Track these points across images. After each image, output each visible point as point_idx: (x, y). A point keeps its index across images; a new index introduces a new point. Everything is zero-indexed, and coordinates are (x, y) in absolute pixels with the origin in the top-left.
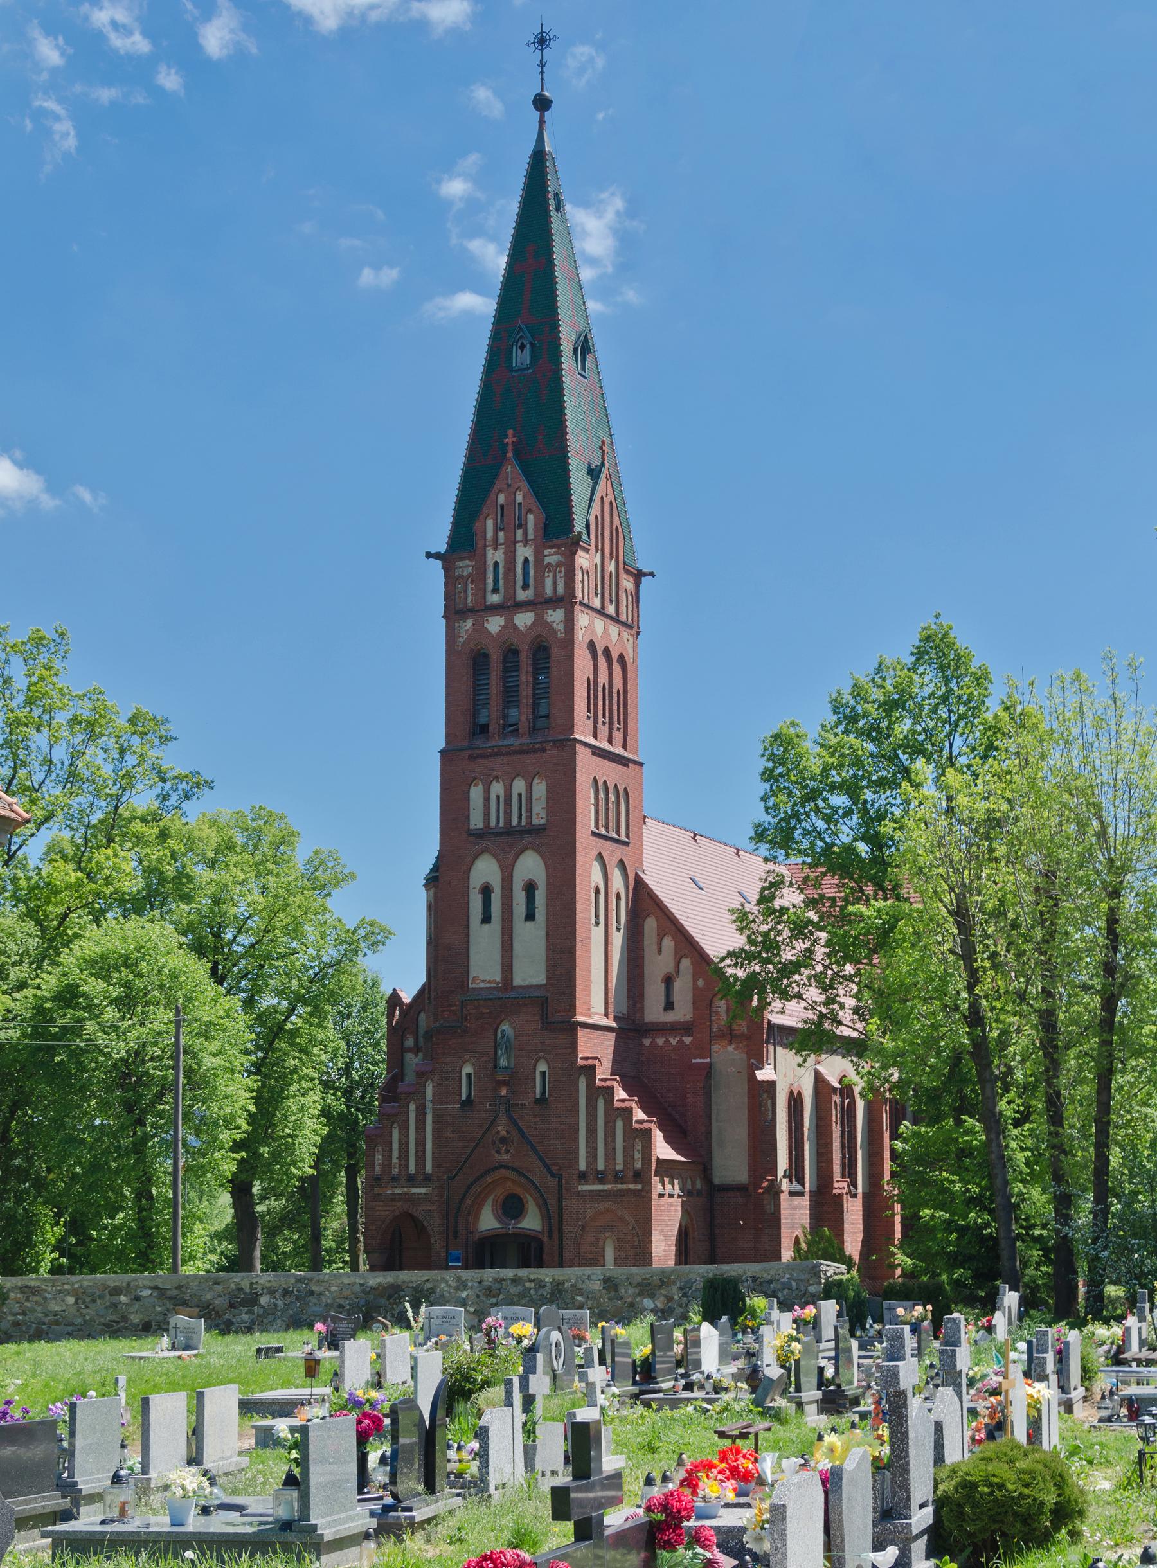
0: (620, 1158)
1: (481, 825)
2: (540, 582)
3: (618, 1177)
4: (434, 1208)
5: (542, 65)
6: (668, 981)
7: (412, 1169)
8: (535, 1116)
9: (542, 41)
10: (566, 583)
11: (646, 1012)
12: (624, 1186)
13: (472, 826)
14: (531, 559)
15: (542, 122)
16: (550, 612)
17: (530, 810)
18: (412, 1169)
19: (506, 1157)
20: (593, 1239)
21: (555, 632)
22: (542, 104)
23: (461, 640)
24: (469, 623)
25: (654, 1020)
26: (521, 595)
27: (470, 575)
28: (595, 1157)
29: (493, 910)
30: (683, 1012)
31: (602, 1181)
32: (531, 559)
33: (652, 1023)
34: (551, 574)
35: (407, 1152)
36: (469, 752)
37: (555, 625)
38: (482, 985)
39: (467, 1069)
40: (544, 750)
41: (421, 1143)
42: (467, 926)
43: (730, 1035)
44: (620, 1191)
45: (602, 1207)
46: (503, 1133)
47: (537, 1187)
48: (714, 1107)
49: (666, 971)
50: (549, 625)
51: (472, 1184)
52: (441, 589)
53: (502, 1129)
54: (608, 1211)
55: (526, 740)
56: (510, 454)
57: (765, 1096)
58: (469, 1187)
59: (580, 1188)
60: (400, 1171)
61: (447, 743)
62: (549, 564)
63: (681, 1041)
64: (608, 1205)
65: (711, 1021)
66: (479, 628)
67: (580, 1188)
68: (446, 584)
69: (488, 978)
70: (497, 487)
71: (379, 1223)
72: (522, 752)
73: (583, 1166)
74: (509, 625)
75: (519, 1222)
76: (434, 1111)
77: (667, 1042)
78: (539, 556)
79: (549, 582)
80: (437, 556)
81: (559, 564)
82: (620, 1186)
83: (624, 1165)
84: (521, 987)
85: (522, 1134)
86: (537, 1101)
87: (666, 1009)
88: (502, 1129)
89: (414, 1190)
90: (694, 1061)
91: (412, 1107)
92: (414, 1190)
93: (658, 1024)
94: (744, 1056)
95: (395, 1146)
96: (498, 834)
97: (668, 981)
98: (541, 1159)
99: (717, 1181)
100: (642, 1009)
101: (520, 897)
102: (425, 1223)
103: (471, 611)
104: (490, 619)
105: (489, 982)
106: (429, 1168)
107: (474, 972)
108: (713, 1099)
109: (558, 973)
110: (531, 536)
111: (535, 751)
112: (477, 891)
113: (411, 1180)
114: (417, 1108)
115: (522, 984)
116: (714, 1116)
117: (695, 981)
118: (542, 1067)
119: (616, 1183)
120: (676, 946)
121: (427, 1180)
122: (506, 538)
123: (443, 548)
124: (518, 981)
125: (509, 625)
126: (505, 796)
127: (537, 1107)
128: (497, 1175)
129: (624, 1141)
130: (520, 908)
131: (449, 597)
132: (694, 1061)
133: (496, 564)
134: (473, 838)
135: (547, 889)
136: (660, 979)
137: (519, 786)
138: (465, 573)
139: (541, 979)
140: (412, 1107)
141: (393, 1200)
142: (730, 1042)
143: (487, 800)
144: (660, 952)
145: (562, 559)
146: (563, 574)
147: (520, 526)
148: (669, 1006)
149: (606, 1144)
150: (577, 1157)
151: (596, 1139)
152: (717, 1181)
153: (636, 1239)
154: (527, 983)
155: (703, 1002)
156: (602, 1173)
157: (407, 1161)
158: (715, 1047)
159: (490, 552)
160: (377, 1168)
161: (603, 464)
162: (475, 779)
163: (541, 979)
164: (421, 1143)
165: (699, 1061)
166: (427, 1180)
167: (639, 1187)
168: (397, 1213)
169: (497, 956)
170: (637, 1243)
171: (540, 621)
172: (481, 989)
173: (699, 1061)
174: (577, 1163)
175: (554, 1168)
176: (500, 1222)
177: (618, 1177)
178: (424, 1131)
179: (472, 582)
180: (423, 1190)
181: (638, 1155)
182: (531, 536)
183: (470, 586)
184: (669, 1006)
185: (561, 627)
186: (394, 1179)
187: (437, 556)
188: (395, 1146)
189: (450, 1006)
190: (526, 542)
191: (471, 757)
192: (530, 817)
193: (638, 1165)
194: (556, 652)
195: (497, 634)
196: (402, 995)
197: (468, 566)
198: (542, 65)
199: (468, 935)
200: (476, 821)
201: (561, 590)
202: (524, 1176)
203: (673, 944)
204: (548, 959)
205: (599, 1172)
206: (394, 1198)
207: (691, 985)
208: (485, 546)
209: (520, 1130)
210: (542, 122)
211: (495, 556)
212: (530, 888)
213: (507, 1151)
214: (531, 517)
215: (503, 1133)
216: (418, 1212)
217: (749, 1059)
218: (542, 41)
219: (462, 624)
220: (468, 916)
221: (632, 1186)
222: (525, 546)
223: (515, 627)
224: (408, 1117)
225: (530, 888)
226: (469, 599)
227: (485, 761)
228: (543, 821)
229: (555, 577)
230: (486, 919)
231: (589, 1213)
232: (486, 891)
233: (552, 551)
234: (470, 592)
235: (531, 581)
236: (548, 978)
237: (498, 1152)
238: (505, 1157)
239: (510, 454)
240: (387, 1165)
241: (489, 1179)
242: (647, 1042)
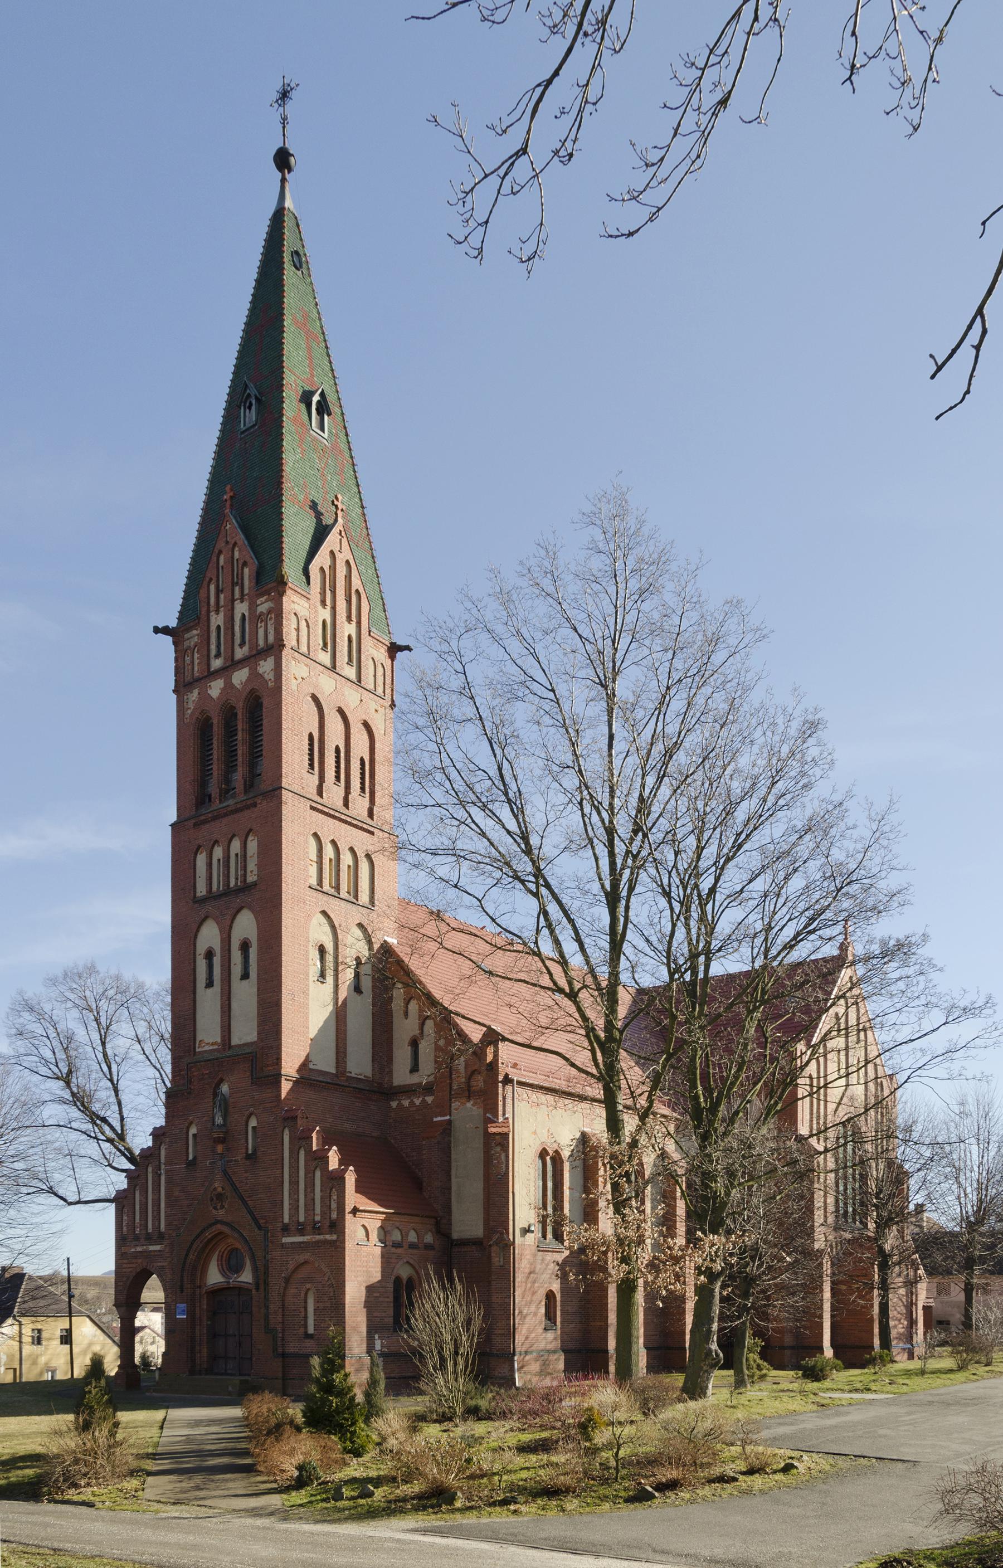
3: (317, 1229)
5: (284, 121)
6: (414, 1043)
9: (284, 95)
11: (395, 1075)
12: (321, 1237)
14: (247, 614)
15: (283, 180)
16: (262, 663)
17: (245, 868)
19: (222, 1212)
20: (295, 1291)
22: (283, 160)
23: (189, 712)
24: (196, 692)
25: (402, 1083)
29: (215, 973)
30: (426, 1073)
31: (301, 1232)
32: (247, 614)
33: (400, 1086)
38: (207, 1048)
39: (193, 1130)
40: (255, 805)
43: (469, 1093)
44: (318, 1242)
46: (220, 1189)
48: (453, 1164)
49: (412, 1034)
53: (218, 1185)
55: (243, 797)
57: (498, 1149)
58: (192, 1244)
63: (424, 1101)
65: (451, 1079)
66: (204, 696)
69: (211, 1041)
74: (229, 685)
77: (412, 1103)
78: (253, 607)
79: (261, 632)
80: (165, 631)
82: (318, 1237)
84: (239, 1046)
85: (235, 1189)
87: (412, 1071)
89: (152, 1248)
90: (435, 1119)
92: (152, 1248)
93: (404, 1086)
94: (481, 1111)
97: (414, 1043)
98: (251, 1213)
99: (455, 1236)
100: (391, 1073)
101: (237, 956)
103: (198, 680)
108: (453, 1156)
109: (267, 1027)
111: (248, 807)
112: (202, 956)
113: (149, 1239)
116: (453, 1172)
118: (253, 1123)
119: (314, 1234)
121: (161, 1237)
123: (173, 623)
124: (235, 1041)
125: (229, 685)
127: (248, 1163)
130: (237, 970)
131: (179, 671)
132: (435, 1119)
133: (219, 627)
136: (407, 1042)
137: (236, 846)
138: (192, 643)
141: (136, 1257)
142: (469, 1098)
143: (210, 865)
148: (415, 1069)
149: (305, 1195)
152: (455, 1236)
153: (331, 1289)
155: (445, 1061)
158: (455, 1105)
159: (213, 615)
161: (336, 520)
162: (199, 847)
165: (439, 1119)
167: (334, 1237)
169: (218, 1018)
171: (255, 675)
172: (206, 1051)
173: (439, 1119)
175: (262, 1221)
180: (158, 1248)
183: (196, 655)
184: (415, 1069)
187: (165, 631)
193: (334, 1215)
194: (266, 702)
195: (218, 698)
198: (284, 121)
201: (271, 638)
204: (259, 1015)
205: (299, 1224)
208: (208, 612)
209: (233, 1184)
210: (283, 180)
211: (217, 620)
212: (245, 946)
213: (222, 1207)
215: (220, 1189)
217: (485, 1114)
218: (284, 95)
219: (190, 695)
221: (328, 1237)
223: (232, 686)
225: (245, 946)
226: (196, 669)
227: (207, 826)
228: (255, 878)
230: (210, 984)
232: (209, 955)
233: (263, 599)
234: (196, 661)
237: (215, 1208)
242: (394, 1104)
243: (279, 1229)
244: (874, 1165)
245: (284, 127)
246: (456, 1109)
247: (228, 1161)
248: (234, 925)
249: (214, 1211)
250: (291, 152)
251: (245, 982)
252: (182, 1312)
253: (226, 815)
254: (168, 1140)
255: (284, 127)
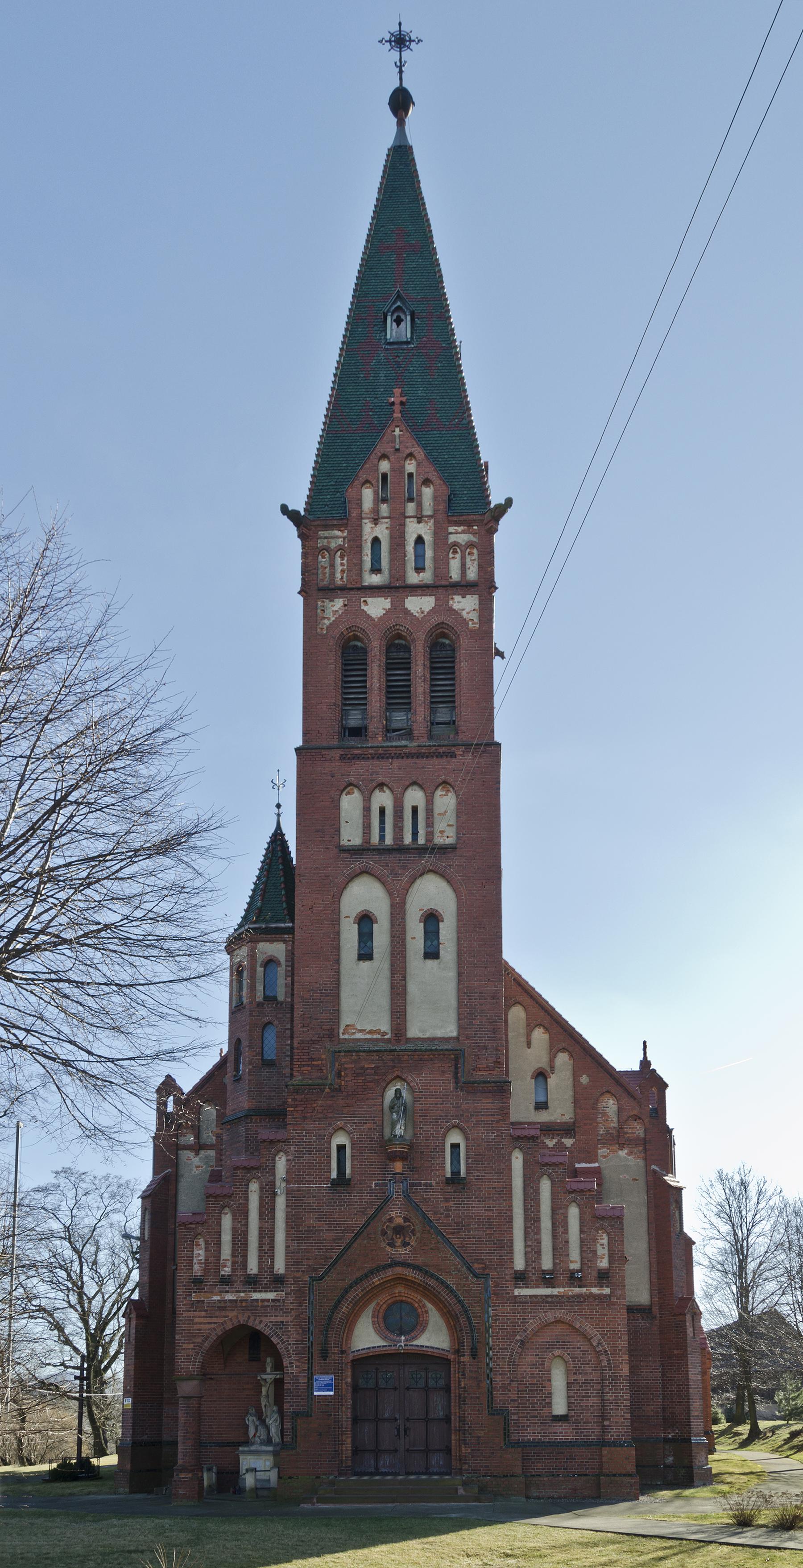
0: (575, 1254)
1: (357, 841)
2: (441, 564)
3: (573, 1279)
4: (290, 1319)
7: (253, 1267)
8: (447, 1200)
9: (400, 41)
10: (480, 566)
12: (584, 1290)
13: (344, 842)
14: (428, 538)
16: (457, 598)
18: (253, 1267)
21: (465, 622)
23: (327, 622)
24: (338, 604)
26: (413, 578)
27: (340, 548)
28: (539, 1253)
32: (428, 538)
34: (458, 556)
35: (246, 1244)
36: (341, 752)
37: (464, 614)
40: (453, 755)
41: (267, 1234)
42: (338, 961)
44: (579, 1296)
45: (550, 1316)
46: (400, 1221)
47: (452, 1291)
50: (456, 613)
51: (351, 1286)
52: (299, 561)
54: (558, 1322)
56: (397, 415)
58: (346, 1291)
59: (517, 1292)
60: (234, 1270)
61: (304, 741)
62: (455, 544)
63: (560, 1143)
64: (559, 1314)
67: (517, 1292)
68: (304, 555)
69: (368, 1028)
70: (380, 449)
71: (199, 1340)
72: (419, 755)
73: (519, 1264)
75: (415, 1338)
76: (289, 1192)
78: (440, 536)
81: (471, 545)
82: (577, 1290)
83: (582, 1264)
84: (418, 1039)
86: (449, 1182)
88: (396, 1215)
89: (256, 1296)
90: (577, 1165)
91: (254, 1187)
92: (256, 1296)
94: (641, 1163)
95: (226, 1238)
96: (382, 851)
101: (415, 931)
102: (275, 1340)
104: (369, 600)
105: (370, 1032)
106: (280, 1266)
107: (346, 1019)
110: (428, 510)
111: (440, 756)
112: (352, 920)
113: (252, 1282)
114: (261, 1189)
115: (420, 1035)
117: (576, 1077)
120: (551, 1039)
121: (278, 1281)
122: (392, 511)
124: (414, 1031)
125: (398, 608)
126: (395, 807)
127: (449, 1189)
128: (390, 1273)
129: (582, 1232)
131: (308, 570)
133: (376, 541)
134: (346, 855)
135: (459, 920)
136: (530, 1074)
139: (451, 1030)
140: (254, 1187)
144: (529, 1045)
145: (475, 540)
146: (475, 556)
147: (411, 500)
150: (511, 1252)
151: (538, 1231)
154: (427, 1035)
156: (550, 1272)
157: (245, 1257)
160: (196, 1267)
163: (451, 1030)
164: (267, 1234)
165: (584, 1165)
166: (278, 1281)
167: (607, 1291)
168: (229, 1326)
170: (605, 1363)
172: (359, 1040)
173: (584, 1165)
174: (511, 1260)
175: (476, 1266)
176: (385, 1338)
177: (573, 1279)
178: (273, 1218)
179: (342, 557)
180: (271, 1296)
181: (602, 1251)
182: (428, 510)
183: (338, 560)
185: (474, 616)
186: (226, 1281)
188: (226, 1238)
189: (313, 1059)
190: (420, 519)
191: (343, 758)
192: (430, 835)
194: (465, 645)
195: (380, 619)
196: (180, 1082)
197: (338, 537)
199: (338, 972)
200: (351, 835)
201: (472, 574)
202: (432, 1276)
203: (546, 1036)
205: (544, 1272)
206: (223, 1306)
207: (570, 1082)
212: (432, 919)
213: (405, 1244)
214: (428, 492)
216: (263, 1324)
220: (338, 948)
221: (595, 1290)
222: (419, 522)
223: (407, 612)
224: (247, 1199)
225: (432, 919)
228: (450, 841)
229: (463, 558)
230: (365, 955)
231: (532, 1325)
232: (365, 920)
233: (460, 529)
234: (339, 568)
235: (429, 563)
236: (460, 1027)
237: (392, 1245)
238: (402, 1253)
239: (397, 415)
240: (213, 1262)
241: (376, 1280)
243: (508, 1277)
244: (196, 1327)
245: (401, 72)
246: (605, 1157)
247: (412, 1185)
248: (345, 893)
249: (388, 1249)
250: (414, 100)
251: (365, 965)
252: (327, 1387)
253: (400, 756)
254: (292, 1148)
255: (401, 72)
